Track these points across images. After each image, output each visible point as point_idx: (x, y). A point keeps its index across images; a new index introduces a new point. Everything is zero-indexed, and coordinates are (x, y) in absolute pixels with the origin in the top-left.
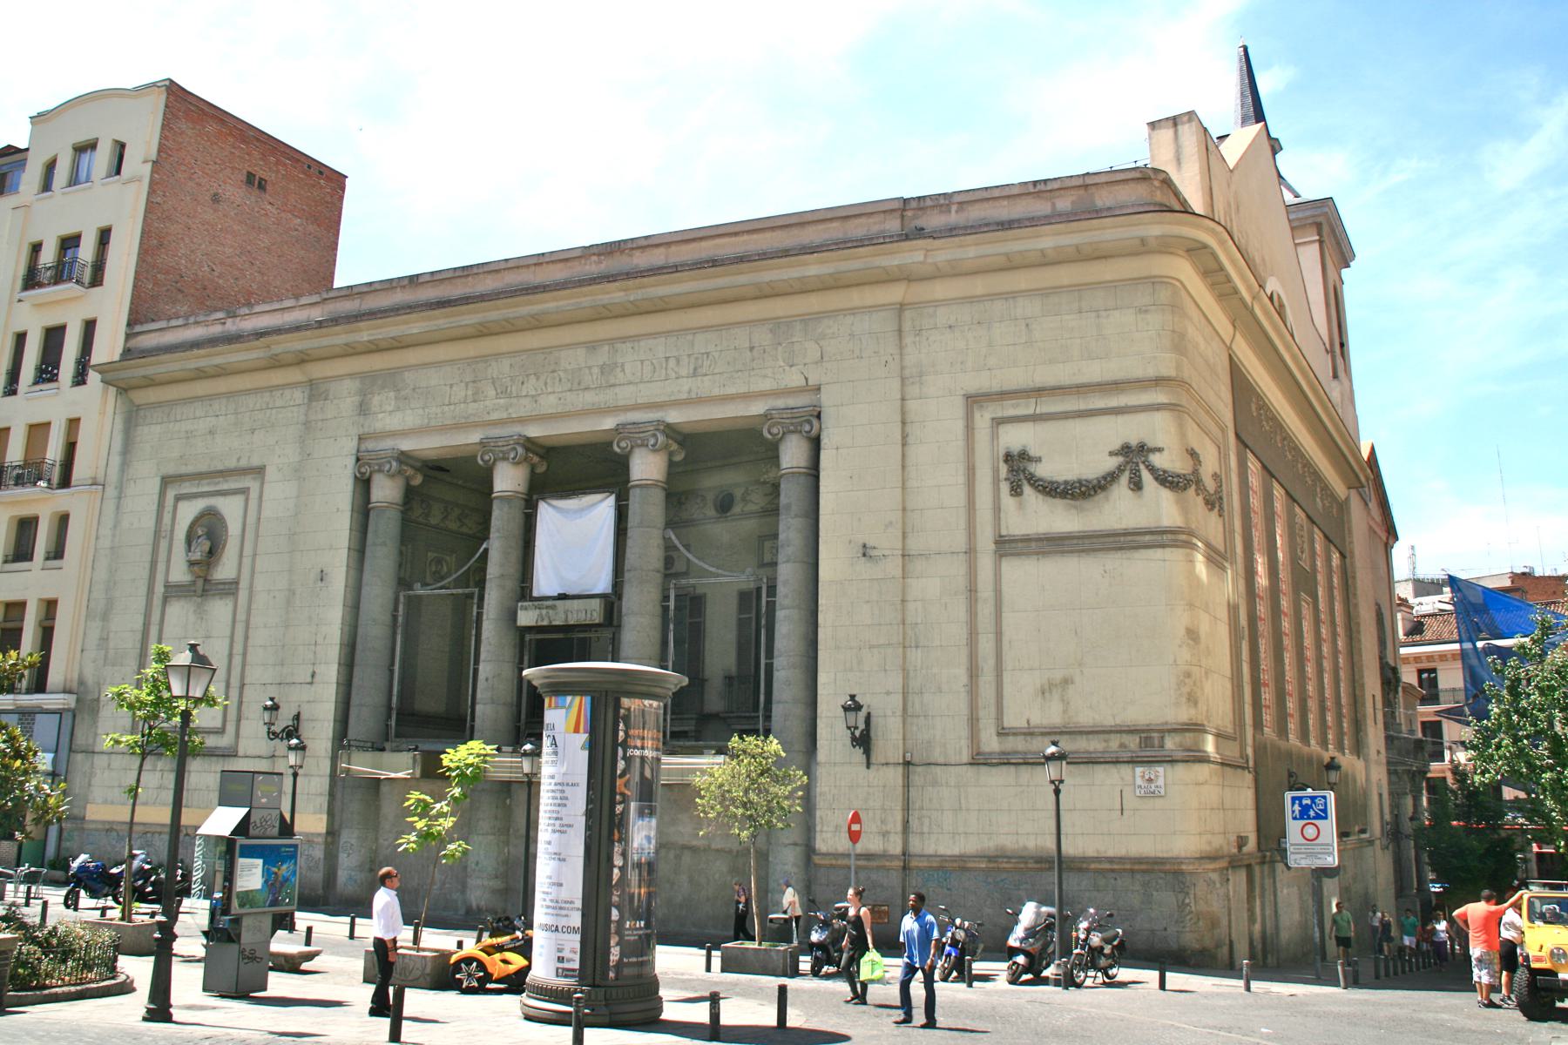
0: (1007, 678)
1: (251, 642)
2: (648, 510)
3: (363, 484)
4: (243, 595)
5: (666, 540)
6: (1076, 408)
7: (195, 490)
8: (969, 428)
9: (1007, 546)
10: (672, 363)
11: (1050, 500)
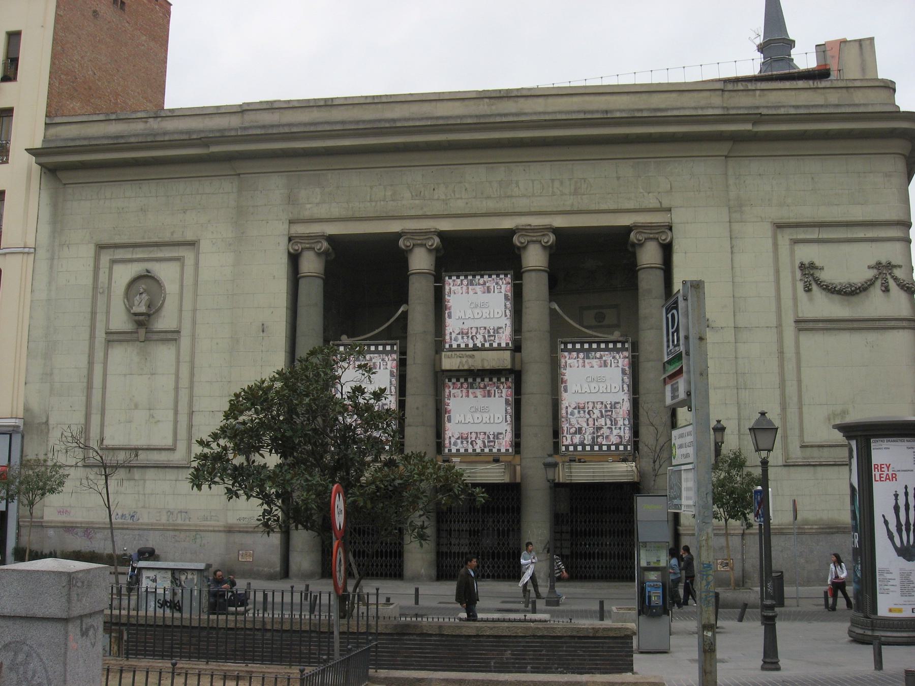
0: (805, 409)
1: (196, 379)
2: (536, 287)
3: (294, 259)
4: (185, 342)
5: (552, 312)
6: (845, 236)
7: (129, 256)
8: (775, 245)
9: (804, 325)
10: (557, 184)
11: (830, 295)
